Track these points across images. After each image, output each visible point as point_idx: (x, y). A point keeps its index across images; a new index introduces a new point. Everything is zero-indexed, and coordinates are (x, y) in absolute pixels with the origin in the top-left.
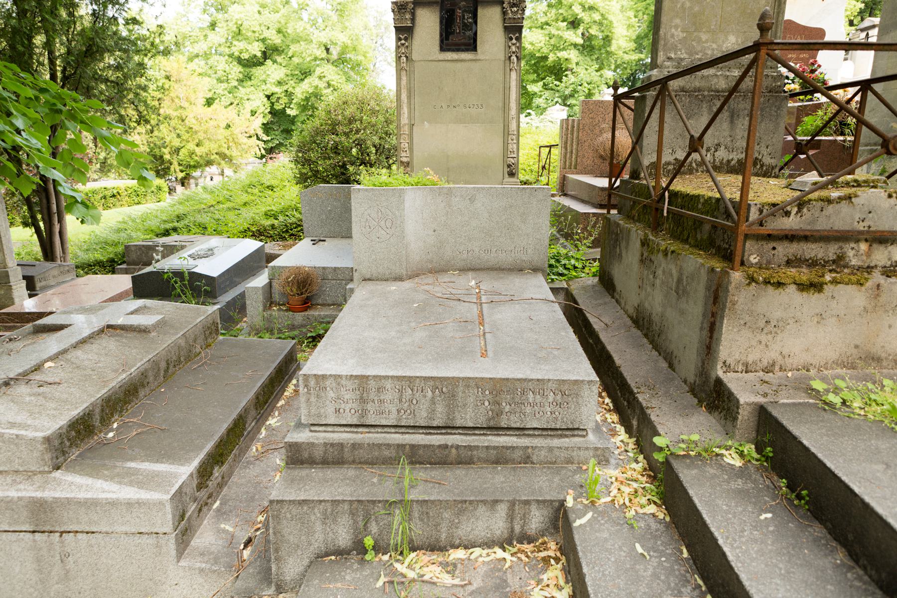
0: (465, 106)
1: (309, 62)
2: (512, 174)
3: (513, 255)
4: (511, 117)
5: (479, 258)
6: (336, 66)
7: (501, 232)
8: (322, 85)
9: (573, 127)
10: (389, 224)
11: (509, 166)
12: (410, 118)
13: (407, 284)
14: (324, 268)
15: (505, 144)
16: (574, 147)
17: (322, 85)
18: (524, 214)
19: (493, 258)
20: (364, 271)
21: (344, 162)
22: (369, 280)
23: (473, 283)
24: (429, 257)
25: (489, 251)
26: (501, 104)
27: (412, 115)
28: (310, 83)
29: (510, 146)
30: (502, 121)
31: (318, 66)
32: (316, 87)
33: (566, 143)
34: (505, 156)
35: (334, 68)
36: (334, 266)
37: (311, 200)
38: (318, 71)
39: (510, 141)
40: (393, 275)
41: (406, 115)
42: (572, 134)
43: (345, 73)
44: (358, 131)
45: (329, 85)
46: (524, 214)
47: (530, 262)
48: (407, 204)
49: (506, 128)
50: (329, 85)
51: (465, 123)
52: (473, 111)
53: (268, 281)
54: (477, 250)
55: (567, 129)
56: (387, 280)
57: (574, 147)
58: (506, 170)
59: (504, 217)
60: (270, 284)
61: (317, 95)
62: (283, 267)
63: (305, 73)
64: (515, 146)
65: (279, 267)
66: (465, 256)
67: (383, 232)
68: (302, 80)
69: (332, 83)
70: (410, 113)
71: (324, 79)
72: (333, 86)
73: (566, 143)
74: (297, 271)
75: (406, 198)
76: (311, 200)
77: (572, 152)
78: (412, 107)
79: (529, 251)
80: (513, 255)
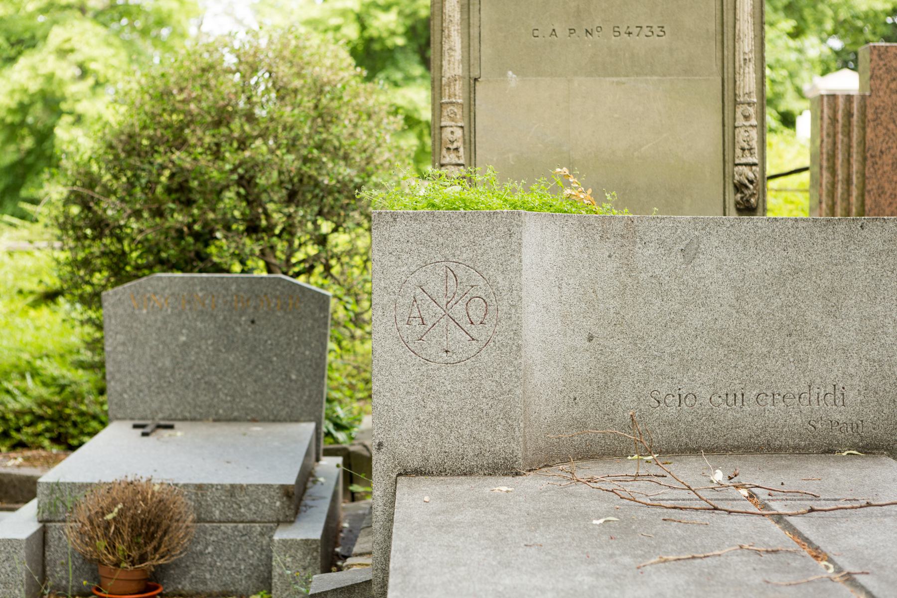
0: (616, 31)
1: (31, 16)
2: (747, 209)
3: (806, 409)
4: (740, 57)
5: (711, 418)
6: (105, 25)
7: (772, 344)
8: (66, 71)
9: (849, 115)
10: (476, 313)
11: (739, 187)
12: (467, 61)
13: (531, 483)
14: (200, 487)
15: (728, 130)
16: (855, 167)
17: (66, 71)
18: (833, 291)
19: (748, 417)
20: (402, 449)
21: (206, 224)
22: (418, 472)
23: (719, 476)
24: (576, 412)
25: (736, 397)
26: (713, 26)
27: (474, 54)
28: (34, 68)
29: (741, 135)
30: (716, 68)
31: (55, 22)
32: (50, 78)
33: (832, 157)
34: (727, 161)
35: (101, 30)
36: (228, 481)
37: (132, 315)
38: (57, 36)
39: (740, 121)
40: (488, 459)
41: (458, 54)
42: (848, 134)
43: (129, 44)
44: (243, 144)
45: (84, 73)
46: (833, 291)
47: (855, 427)
48: (529, 255)
49: (729, 86)
50: (84, 73)
51: (617, 75)
52: (640, 44)
53: (35, 527)
54: (704, 393)
55: (834, 120)
56: (468, 473)
57: (855, 167)
58: (732, 198)
59: (777, 302)
60: (42, 538)
61: (52, 103)
62: (83, 486)
63: (20, 42)
64: (754, 133)
65: (74, 487)
66: (673, 410)
67: (459, 334)
68: (11, 60)
69: (92, 66)
70: (467, 47)
71: (72, 57)
72: (95, 73)
73: (832, 157)
74: (129, 493)
75: (526, 238)
76: (132, 315)
77: (848, 181)
78: (474, 31)
79: (851, 395)
80: (806, 409)
